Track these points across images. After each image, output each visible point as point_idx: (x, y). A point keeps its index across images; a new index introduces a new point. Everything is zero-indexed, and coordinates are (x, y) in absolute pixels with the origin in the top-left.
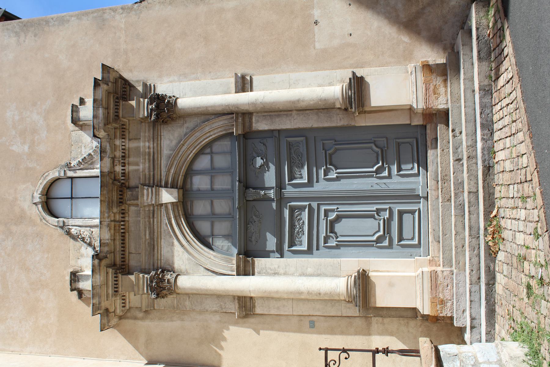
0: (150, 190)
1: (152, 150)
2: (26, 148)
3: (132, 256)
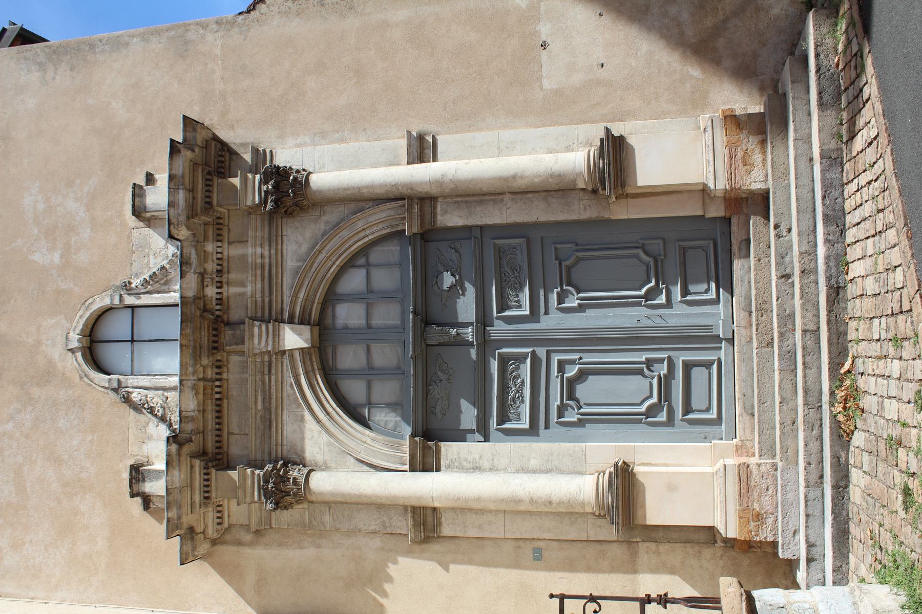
1: (267, 260)
2: (56, 257)
3: (233, 439)
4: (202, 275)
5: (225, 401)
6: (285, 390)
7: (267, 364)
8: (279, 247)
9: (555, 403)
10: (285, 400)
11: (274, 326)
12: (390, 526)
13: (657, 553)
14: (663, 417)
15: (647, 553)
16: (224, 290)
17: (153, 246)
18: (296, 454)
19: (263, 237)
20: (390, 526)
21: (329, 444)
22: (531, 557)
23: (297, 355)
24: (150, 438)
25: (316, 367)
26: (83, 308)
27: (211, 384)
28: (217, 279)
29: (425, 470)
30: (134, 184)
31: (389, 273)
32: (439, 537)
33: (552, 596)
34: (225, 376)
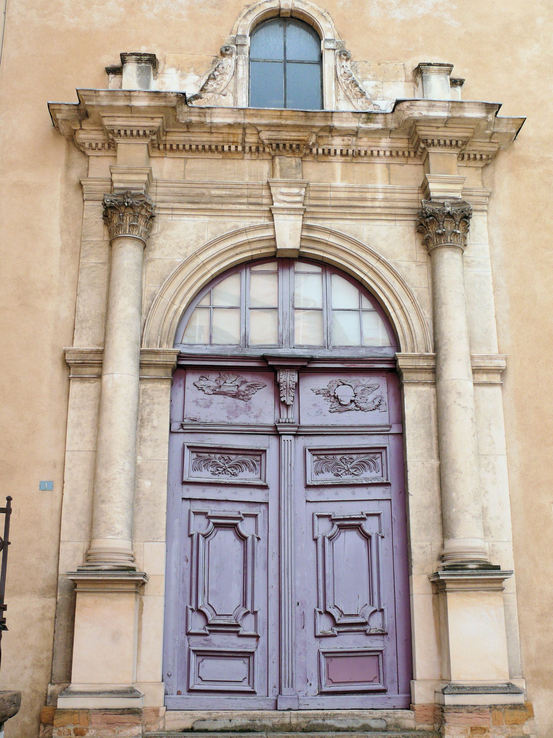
0: (298, 199)
1: (369, 204)
3: (181, 163)
4: (355, 133)
5: (221, 156)
6: (231, 219)
7: (259, 201)
8: (383, 218)
9: (213, 509)
10: (220, 219)
11: (299, 209)
12: (82, 328)
13: (42, 619)
14: (197, 624)
15: (43, 607)
16: (339, 158)
17: (385, 84)
18: (163, 229)
19: (394, 200)
20: (82, 328)
21: (172, 264)
22: (45, 479)
23: (268, 233)
24: (183, 76)
25: (254, 253)
26: (322, 10)
27: (240, 141)
28: (350, 152)
29: (142, 366)
30: (452, 66)
31: (358, 332)
32: (69, 379)
33: (9, 499)
34: (247, 156)
